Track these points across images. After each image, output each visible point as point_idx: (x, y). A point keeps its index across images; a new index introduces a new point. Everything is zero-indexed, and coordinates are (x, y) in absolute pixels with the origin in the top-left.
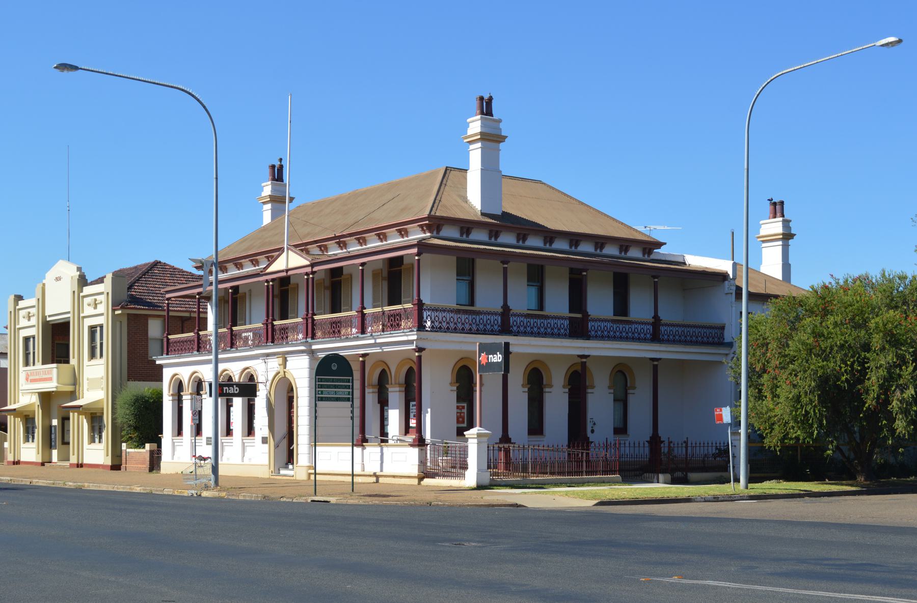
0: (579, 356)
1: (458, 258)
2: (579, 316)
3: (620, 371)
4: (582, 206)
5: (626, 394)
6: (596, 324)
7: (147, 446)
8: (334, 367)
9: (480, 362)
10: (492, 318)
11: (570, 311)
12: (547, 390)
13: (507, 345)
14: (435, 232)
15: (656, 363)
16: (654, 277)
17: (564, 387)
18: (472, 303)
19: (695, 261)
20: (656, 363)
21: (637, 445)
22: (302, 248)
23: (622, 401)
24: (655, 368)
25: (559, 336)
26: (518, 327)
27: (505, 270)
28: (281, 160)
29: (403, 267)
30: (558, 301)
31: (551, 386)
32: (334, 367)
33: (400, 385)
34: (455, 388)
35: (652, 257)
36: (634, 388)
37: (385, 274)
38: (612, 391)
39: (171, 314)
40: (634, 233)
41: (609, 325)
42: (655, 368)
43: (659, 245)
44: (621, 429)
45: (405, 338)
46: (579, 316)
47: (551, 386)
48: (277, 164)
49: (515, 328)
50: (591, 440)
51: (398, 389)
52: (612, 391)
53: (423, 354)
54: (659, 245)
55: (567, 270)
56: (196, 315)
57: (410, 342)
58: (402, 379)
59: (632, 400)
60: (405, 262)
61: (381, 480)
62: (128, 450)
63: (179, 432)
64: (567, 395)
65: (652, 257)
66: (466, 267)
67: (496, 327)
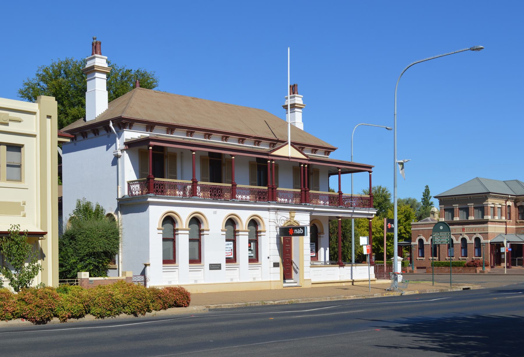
9: (387, 227)
12: (322, 236)
45: (367, 212)
57: (372, 214)
61: (355, 283)
62: (91, 279)
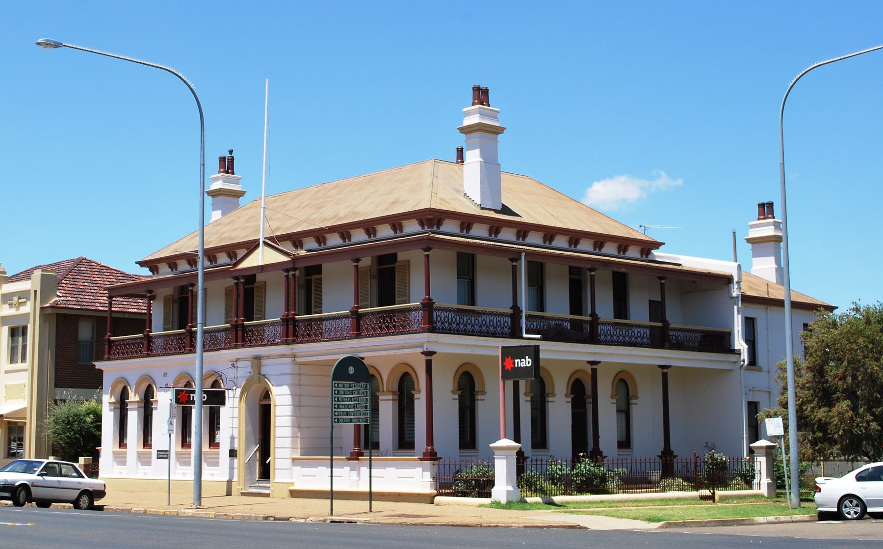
0: (589, 362)
1: (458, 253)
2: (660, 324)
3: (622, 380)
4: (572, 202)
5: (628, 404)
6: (606, 328)
7: (82, 460)
8: (351, 370)
10: (642, 331)
11: (615, 317)
12: (480, 397)
13: (537, 348)
14: (435, 227)
15: (665, 371)
16: (661, 278)
17: (453, 392)
18: (542, 309)
19: (692, 262)
20: (665, 371)
21: (648, 461)
22: (274, 242)
23: (625, 413)
24: (665, 377)
25: (641, 345)
26: (606, 336)
27: (662, 285)
28: (231, 152)
29: (397, 264)
30: (558, 305)
31: (554, 395)
32: (351, 370)
33: (394, 393)
34: (570, 400)
35: (650, 258)
36: (637, 398)
37: (375, 272)
38: (614, 401)
39: (114, 315)
40: (631, 232)
41: (451, 315)
42: (665, 377)
43: (657, 245)
44: (625, 443)
46: (660, 324)
47: (554, 395)
48: (227, 155)
49: (439, 324)
50: (675, 454)
51: (391, 397)
52: (614, 401)
53: (433, 357)
54: (657, 245)
55: (566, 270)
56: (107, 315)
58: (395, 387)
59: (636, 411)
60: (399, 259)
63: (122, 443)
64: (570, 405)
65: (650, 258)
66: (467, 264)
67: (506, 330)
